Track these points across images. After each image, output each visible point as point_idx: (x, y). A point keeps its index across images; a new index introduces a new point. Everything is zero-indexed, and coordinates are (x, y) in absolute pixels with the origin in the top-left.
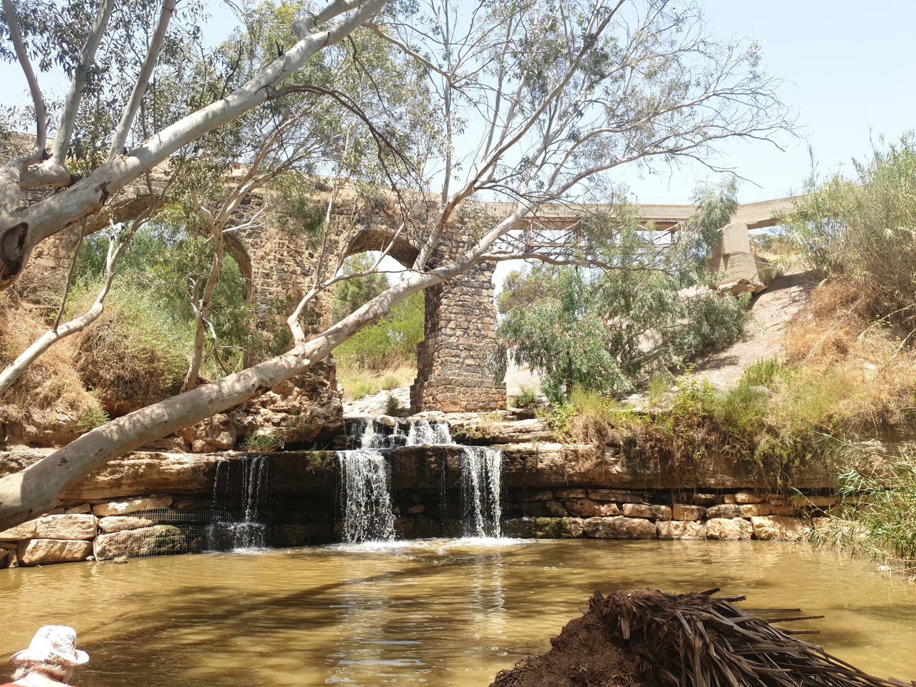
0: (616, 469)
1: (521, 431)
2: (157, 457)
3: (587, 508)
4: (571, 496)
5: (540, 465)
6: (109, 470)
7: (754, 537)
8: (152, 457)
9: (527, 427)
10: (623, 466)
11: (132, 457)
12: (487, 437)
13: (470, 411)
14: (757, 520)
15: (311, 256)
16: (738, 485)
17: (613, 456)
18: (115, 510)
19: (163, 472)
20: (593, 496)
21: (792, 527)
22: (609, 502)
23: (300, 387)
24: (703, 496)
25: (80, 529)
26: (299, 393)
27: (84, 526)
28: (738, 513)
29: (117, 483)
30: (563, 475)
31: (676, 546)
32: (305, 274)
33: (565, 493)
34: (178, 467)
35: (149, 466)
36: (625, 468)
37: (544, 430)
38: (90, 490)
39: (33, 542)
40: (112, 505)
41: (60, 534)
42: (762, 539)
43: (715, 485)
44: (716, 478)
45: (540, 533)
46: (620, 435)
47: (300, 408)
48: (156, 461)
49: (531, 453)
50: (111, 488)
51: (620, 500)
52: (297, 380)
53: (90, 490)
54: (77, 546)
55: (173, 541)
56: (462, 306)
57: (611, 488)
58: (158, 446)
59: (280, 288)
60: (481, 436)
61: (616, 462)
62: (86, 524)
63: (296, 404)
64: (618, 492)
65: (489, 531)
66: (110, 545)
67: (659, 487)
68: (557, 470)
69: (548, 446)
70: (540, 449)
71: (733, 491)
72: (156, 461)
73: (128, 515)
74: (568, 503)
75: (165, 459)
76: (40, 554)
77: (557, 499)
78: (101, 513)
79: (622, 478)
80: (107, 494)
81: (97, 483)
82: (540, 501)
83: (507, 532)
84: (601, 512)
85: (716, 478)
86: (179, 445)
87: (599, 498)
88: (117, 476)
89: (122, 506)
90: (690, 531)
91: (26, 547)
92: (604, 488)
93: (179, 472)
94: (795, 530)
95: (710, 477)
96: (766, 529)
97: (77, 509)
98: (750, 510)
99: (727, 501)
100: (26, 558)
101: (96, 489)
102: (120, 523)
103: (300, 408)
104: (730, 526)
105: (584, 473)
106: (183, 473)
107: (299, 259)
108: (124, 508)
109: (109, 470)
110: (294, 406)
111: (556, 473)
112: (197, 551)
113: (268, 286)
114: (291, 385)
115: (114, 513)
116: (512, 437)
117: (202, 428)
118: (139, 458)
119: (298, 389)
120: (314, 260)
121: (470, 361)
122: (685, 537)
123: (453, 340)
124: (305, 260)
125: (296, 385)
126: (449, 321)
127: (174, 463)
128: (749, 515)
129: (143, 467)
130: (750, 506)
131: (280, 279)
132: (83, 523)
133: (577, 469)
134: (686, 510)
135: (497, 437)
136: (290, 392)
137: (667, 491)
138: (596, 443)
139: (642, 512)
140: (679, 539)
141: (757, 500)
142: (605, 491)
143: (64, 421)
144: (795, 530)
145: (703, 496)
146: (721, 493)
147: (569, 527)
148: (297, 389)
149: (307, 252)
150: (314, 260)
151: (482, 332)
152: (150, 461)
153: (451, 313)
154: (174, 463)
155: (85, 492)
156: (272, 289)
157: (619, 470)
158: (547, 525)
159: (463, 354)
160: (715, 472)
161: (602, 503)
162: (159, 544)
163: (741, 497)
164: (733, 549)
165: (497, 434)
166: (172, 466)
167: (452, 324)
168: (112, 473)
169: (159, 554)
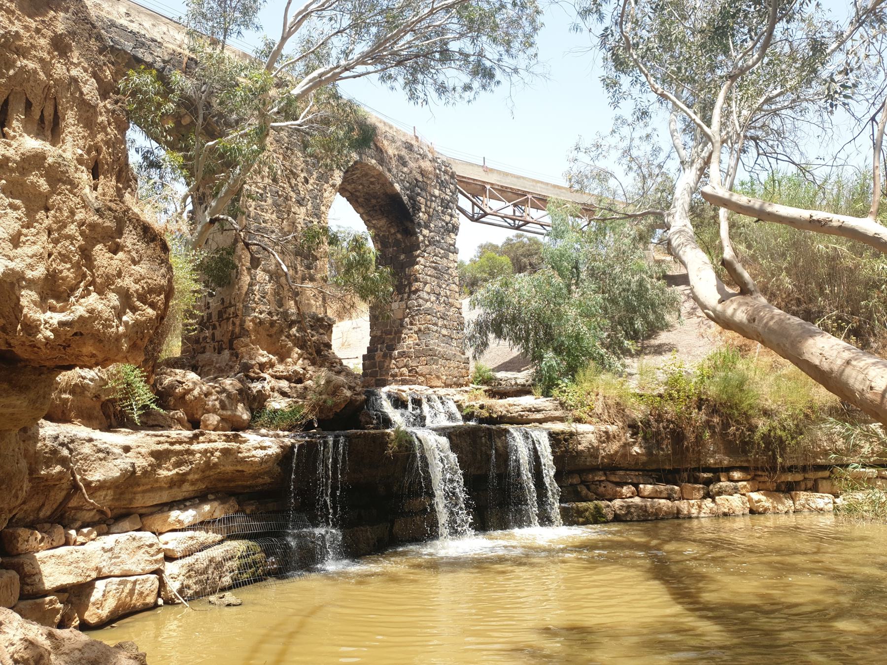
0: (636, 449)
1: (530, 410)
2: (236, 438)
3: (610, 491)
4: (596, 478)
5: (580, 447)
6: (173, 459)
7: (752, 512)
8: (228, 439)
9: (536, 406)
10: (641, 447)
11: (201, 438)
12: (495, 416)
13: (450, 386)
14: (756, 496)
15: (307, 181)
16: (734, 464)
17: (631, 437)
18: (179, 522)
19: (243, 461)
20: (613, 479)
21: (780, 501)
22: (626, 484)
23: (301, 348)
24: (705, 475)
25: (147, 557)
26: (300, 356)
27: (152, 551)
28: (736, 490)
29: (181, 480)
30: (596, 457)
31: (695, 523)
32: (300, 203)
33: (591, 476)
34: (260, 453)
35: (225, 452)
36: (644, 450)
37: (556, 410)
38: (144, 492)
39: (100, 585)
40: (175, 514)
41: (126, 567)
42: (760, 513)
43: (715, 464)
44: (714, 458)
45: (581, 520)
46: (638, 412)
47: (304, 375)
48: (233, 445)
49: (571, 434)
50: (170, 487)
51: (635, 481)
52: (298, 339)
53: (144, 492)
54: (148, 585)
55: (255, 563)
56: (435, 268)
57: (627, 470)
58: (151, 423)
59: (274, 216)
60: (487, 415)
61: (634, 443)
62: (155, 547)
63: (298, 368)
64: (633, 473)
65: (545, 520)
66: (190, 577)
67: (667, 468)
68: (593, 452)
69: (581, 428)
70: (579, 430)
71: (728, 469)
72: (233, 445)
73: (193, 527)
74: (593, 487)
75: (245, 442)
76: (110, 604)
77: (583, 482)
78: (158, 527)
79: (638, 459)
80: (165, 497)
81: (157, 480)
82: (571, 485)
83: (570, 518)
84: (622, 494)
85: (714, 458)
86: (179, 421)
87: (618, 480)
88: (184, 469)
89: (188, 516)
90: (705, 510)
91: (89, 595)
92: (620, 469)
93: (263, 461)
94: (783, 504)
95: (711, 457)
96: (763, 503)
97: (126, 524)
98: (745, 487)
99: (722, 479)
100: (91, 616)
101: (152, 490)
102: (190, 542)
103: (304, 375)
104: (735, 502)
105: (611, 455)
106: (266, 462)
107: (293, 181)
108: (191, 519)
109: (173, 459)
110: (295, 372)
111: (591, 456)
112: (280, 574)
113: (262, 210)
114: (290, 344)
115: (178, 526)
116: (522, 416)
117: (214, 397)
118: (210, 441)
119: (299, 351)
120: (310, 187)
121: (444, 332)
122: (702, 515)
123: (428, 304)
124: (300, 184)
125: (295, 345)
126: (425, 283)
127: (256, 448)
128: (743, 491)
129: (217, 454)
130: (745, 483)
131: (275, 204)
132: (151, 546)
133: (607, 450)
134: (694, 489)
135: (505, 416)
136: (288, 354)
137: (676, 471)
138: (621, 424)
139: (661, 492)
140: (697, 518)
141: (749, 477)
142: (622, 473)
143: (91, 380)
144: (783, 504)
145: (705, 475)
146: (718, 472)
147: (604, 511)
148: (296, 349)
149: (302, 175)
150: (310, 187)
151: (450, 300)
152: (227, 445)
153: (427, 275)
154: (256, 448)
155: (139, 496)
156: (267, 216)
157: (639, 451)
158: (586, 510)
159: (440, 323)
160: (715, 452)
161: (621, 484)
162: (242, 568)
163: (736, 475)
164: (740, 523)
165: (504, 412)
166: (254, 453)
167: (428, 288)
168: (178, 464)
169: (245, 584)
